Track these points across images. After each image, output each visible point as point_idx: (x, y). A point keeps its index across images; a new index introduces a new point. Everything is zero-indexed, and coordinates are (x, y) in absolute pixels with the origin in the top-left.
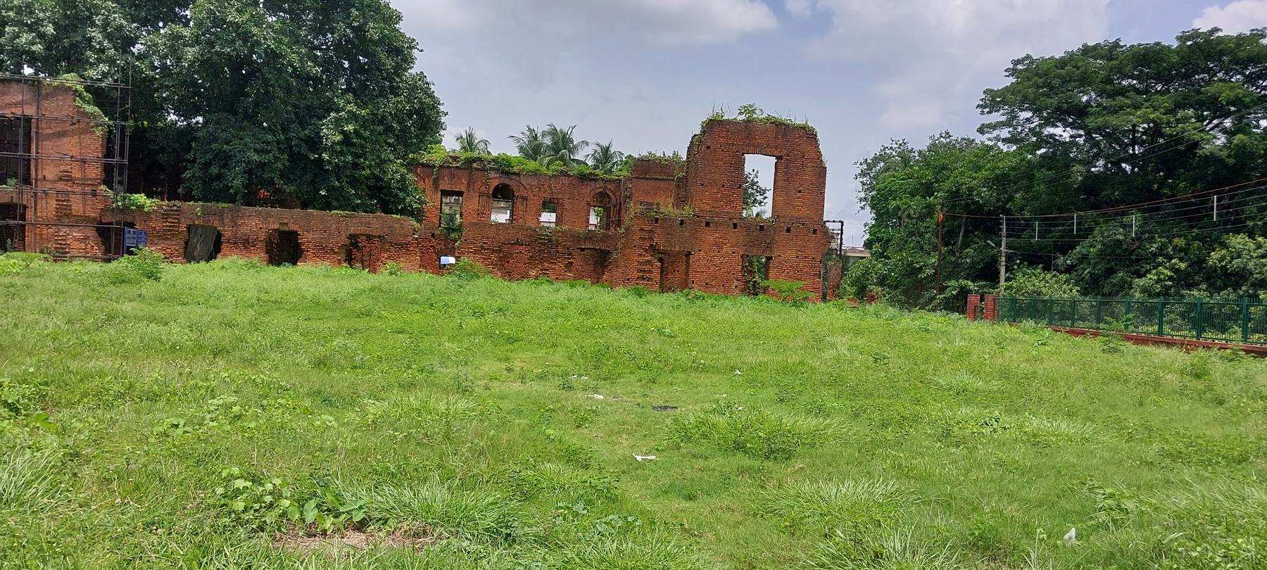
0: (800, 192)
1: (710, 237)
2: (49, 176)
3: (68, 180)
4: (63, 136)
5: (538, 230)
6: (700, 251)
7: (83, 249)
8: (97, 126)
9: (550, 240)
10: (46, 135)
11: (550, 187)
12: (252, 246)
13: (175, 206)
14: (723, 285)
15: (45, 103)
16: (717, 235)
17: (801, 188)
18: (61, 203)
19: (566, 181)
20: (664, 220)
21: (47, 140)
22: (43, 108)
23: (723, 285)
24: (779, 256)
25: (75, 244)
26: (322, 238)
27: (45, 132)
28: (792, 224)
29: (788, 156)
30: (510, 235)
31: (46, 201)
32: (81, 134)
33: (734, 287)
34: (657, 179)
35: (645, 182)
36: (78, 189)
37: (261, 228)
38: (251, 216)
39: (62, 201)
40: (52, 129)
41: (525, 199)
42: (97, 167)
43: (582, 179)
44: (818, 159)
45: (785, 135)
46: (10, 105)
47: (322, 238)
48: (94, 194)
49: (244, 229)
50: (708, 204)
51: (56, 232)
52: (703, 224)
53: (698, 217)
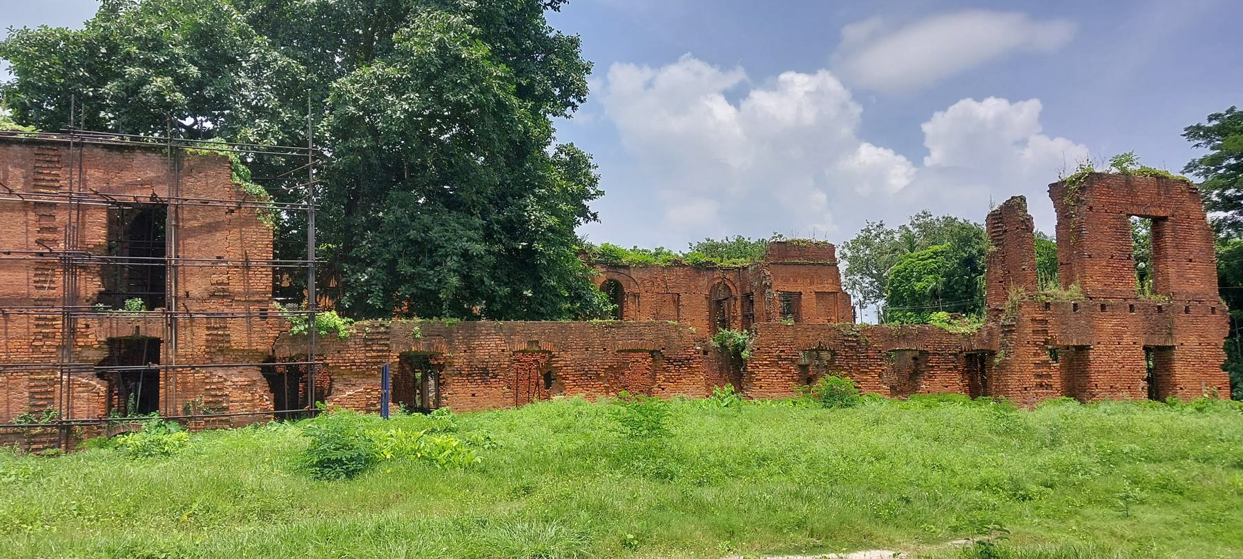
0: (1191, 261)
1: (1108, 325)
2: (195, 292)
3: (224, 297)
4: (216, 231)
5: (842, 329)
6: (1099, 343)
7: (248, 401)
8: (264, 213)
9: (858, 342)
10: (190, 229)
11: (663, 280)
12: (492, 378)
13: (383, 325)
14: (1129, 387)
15: (189, 182)
16: (1114, 322)
17: (1191, 257)
18: (215, 332)
19: (681, 272)
20: (1057, 305)
21: (189, 236)
22: (185, 189)
23: (1129, 387)
24: (1182, 344)
25: (236, 395)
26: (584, 359)
27: (188, 225)
28: (1189, 301)
29: (1173, 216)
30: (811, 338)
31: (192, 330)
32: (242, 225)
33: (1140, 390)
34: (796, 264)
35: (784, 269)
36: (239, 310)
37: (503, 350)
38: (489, 334)
39: (217, 329)
40: (198, 220)
41: (636, 296)
42: (267, 275)
43: (698, 268)
44: (1203, 219)
45: (1167, 191)
46: (133, 186)
47: (584, 359)
48: (264, 316)
49: (480, 354)
50: (1097, 280)
51: (207, 378)
52: (1099, 308)
53: (1091, 298)
